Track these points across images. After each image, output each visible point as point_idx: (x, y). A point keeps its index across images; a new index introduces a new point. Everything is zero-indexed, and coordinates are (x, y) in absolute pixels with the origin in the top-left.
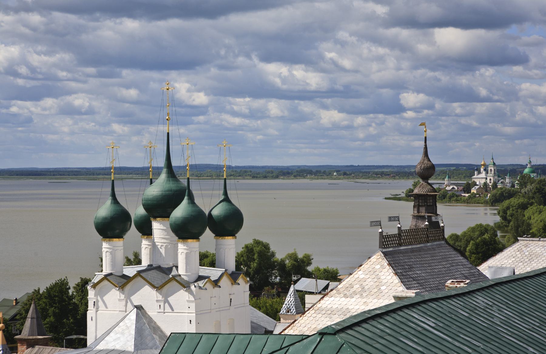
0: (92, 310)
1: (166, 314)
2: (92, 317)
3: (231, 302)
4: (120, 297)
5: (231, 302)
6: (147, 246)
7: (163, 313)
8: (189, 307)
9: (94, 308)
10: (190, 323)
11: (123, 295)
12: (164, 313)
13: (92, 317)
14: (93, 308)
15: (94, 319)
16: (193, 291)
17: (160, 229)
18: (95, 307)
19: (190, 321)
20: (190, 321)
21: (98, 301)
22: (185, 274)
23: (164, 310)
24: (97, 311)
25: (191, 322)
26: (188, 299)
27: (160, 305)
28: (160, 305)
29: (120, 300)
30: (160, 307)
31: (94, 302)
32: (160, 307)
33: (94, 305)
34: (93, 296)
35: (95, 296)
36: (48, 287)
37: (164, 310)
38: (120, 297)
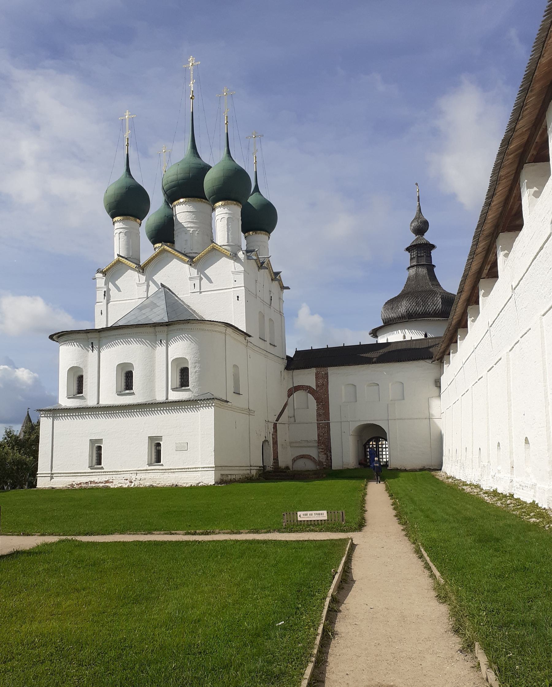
1: (203, 293)
2: (101, 310)
3: (271, 300)
4: (139, 281)
5: (271, 300)
6: (223, 216)
7: (199, 293)
8: (235, 281)
9: (104, 299)
10: (238, 300)
11: (143, 276)
12: (201, 292)
13: (101, 310)
14: (102, 300)
15: (104, 312)
16: (241, 259)
17: (187, 212)
18: (105, 297)
19: (238, 297)
20: (238, 297)
21: (109, 290)
22: (227, 244)
23: (51, 471)
24: (107, 304)
25: (239, 299)
26: (234, 270)
27: (194, 284)
28: (194, 284)
29: (138, 285)
30: (195, 286)
31: (105, 291)
32: (195, 286)
33: (105, 295)
34: (103, 285)
35: (105, 285)
36: (402, 528)
37: (51, 471)
38: (139, 281)
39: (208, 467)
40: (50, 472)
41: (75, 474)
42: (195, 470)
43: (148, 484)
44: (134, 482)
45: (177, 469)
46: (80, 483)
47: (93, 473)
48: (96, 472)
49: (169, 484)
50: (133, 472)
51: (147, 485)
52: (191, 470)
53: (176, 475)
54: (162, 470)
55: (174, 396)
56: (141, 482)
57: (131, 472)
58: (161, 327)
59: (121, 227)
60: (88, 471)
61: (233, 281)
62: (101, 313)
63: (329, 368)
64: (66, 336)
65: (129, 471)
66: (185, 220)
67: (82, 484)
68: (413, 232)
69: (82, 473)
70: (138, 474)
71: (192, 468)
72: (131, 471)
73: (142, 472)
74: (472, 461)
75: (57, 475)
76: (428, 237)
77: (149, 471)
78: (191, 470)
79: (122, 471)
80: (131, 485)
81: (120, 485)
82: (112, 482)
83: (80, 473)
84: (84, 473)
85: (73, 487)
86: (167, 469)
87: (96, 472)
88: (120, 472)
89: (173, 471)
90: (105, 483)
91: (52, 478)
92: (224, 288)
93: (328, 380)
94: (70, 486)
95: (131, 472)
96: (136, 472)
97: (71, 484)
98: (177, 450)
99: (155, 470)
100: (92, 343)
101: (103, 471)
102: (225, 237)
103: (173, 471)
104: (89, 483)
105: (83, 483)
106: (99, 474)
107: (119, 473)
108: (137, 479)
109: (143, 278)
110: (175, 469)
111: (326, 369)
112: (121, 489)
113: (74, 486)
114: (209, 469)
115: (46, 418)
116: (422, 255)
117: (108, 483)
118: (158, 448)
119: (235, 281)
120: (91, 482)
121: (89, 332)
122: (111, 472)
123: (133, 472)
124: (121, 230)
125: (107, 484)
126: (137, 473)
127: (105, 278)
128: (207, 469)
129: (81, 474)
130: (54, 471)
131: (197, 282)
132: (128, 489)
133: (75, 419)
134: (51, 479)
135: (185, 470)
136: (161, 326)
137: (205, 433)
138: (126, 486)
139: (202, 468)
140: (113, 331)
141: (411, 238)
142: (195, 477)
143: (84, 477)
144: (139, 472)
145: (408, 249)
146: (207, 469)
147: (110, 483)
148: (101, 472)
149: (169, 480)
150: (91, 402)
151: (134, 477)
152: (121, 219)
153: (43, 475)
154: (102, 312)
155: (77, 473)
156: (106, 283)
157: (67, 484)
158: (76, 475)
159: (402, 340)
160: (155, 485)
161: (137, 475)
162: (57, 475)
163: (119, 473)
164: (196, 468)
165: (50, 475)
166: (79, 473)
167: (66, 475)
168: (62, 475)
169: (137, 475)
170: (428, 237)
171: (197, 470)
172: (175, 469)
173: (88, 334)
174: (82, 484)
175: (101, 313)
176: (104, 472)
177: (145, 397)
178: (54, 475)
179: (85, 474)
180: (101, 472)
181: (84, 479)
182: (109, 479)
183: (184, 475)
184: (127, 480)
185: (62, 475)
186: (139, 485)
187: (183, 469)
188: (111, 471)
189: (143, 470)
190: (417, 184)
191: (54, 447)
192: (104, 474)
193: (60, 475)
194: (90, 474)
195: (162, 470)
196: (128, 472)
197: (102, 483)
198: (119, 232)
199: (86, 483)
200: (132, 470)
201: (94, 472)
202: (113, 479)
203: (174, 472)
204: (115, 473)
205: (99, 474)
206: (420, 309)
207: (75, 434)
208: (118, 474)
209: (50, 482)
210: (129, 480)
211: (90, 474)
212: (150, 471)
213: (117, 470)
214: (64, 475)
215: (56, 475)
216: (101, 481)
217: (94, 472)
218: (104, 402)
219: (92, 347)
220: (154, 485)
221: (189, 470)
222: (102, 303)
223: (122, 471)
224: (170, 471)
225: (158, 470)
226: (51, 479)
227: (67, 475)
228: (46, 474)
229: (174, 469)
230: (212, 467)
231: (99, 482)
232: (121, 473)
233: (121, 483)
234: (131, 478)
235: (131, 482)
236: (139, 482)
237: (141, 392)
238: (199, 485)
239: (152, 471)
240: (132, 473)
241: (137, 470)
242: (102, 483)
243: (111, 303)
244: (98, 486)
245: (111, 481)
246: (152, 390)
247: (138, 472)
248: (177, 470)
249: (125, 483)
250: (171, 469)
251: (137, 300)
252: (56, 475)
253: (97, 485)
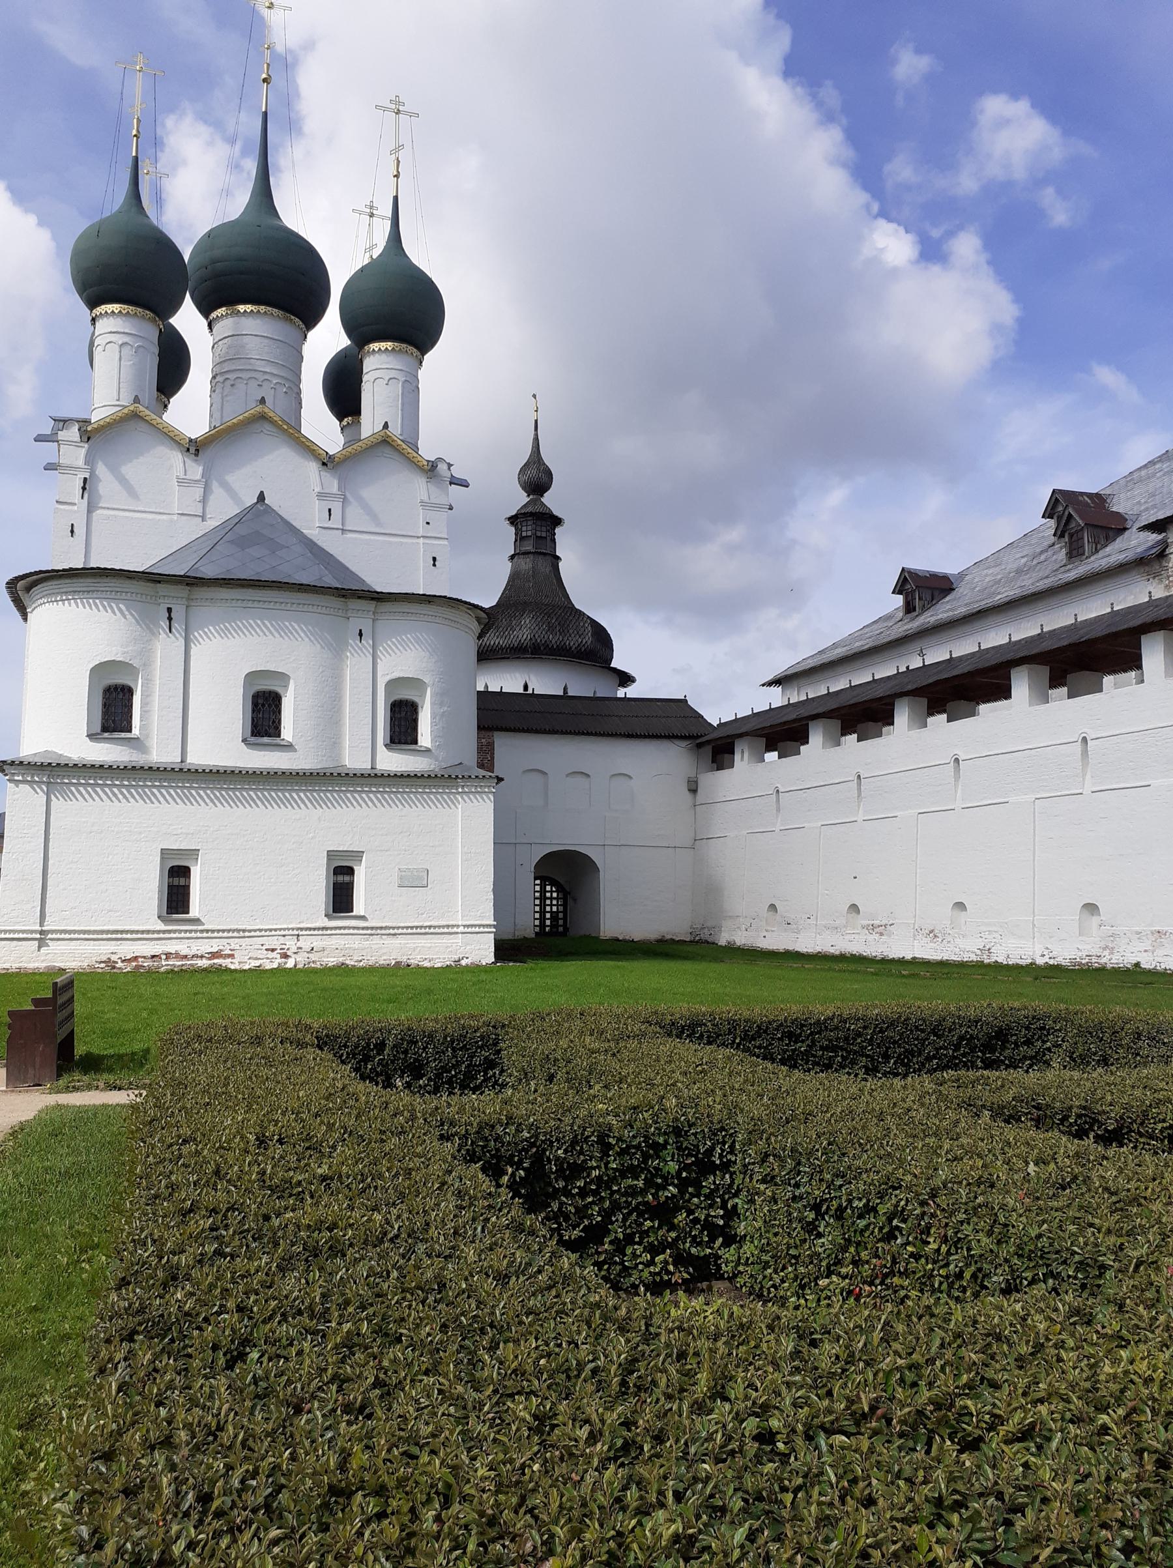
1: (350, 535)
2: (72, 525)
6: (393, 374)
8: (428, 523)
9: (82, 498)
10: (434, 565)
13: (72, 525)
15: (80, 530)
18: (86, 495)
19: (434, 559)
20: (434, 559)
23: (41, 925)
26: (426, 499)
27: (330, 510)
28: (330, 510)
29: (181, 482)
30: (330, 515)
31: (85, 479)
32: (330, 515)
33: (84, 489)
34: (80, 462)
39: (480, 926)
40: (38, 928)
41: (118, 935)
42: (446, 930)
43: (332, 961)
44: (293, 956)
45: (403, 928)
46: (136, 958)
47: (169, 932)
48: (180, 931)
49: (388, 962)
50: (286, 932)
51: (330, 964)
52: (437, 930)
53: (400, 940)
54: (363, 928)
55: (392, 761)
56: (313, 957)
57: (283, 933)
58: (359, 600)
59: (127, 331)
60: (158, 928)
61: (421, 523)
62: (72, 532)
63: (496, 734)
64: (89, 580)
65: (276, 930)
67: (140, 960)
68: (524, 488)
69: (137, 932)
70: (300, 938)
71: (439, 927)
72: (280, 930)
73: (312, 932)
74: (1034, 925)
75: (58, 936)
76: (551, 500)
77: (329, 932)
78: (437, 930)
79: (255, 931)
80: (286, 963)
81: (257, 963)
82: (232, 956)
83: (132, 932)
84: (143, 932)
85: (114, 967)
86: (377, 928)
87: (180, 931)
88: (250, 931)
89: (391, 931)
90: (209, 959)
91: (42, 943)
92: (399, 533)
93: (493, 758)
94: (103, 965)
95: (283, 933)
96: (296, 932)
97: (104, 959)
98: (402, 884)
99: (344, 928)
100: (169, 610)
101: (200, 928)
103: (391, 931)
104: (164, 957)
105: (144, 957)
106: (188, 935)
107: (247, 934)
108: (301, 948)
109: (196, 471)
110: (398, 928)
111: (490, 734)
112: (258, 972)
113: (117, 965)
114: (482, 929)
115: (27, 787)
116: (544, 535)
117: (217, 958)
118: (176, 881)
119: (428, 523)
120: (168, 955)
121: (159, 582)
122: (223, 931)
123: (286, 932)
124: (126, 339)
125: (216, 961)
126: (298, 935)
127: (86, 446)
128: (477, 930)
129: (134, 936)
130: (48, 925)
131: (337, 508)
132: (280, 971)
133: (475, 801)
134: (39, 948)
135: (423, 931)
136: (359, 598)
137: (473, 850)
138: (275, 965)
139: (464, 926)
140: (234, 590)
141: (521, 499)
142: (447, 947)
143: (144, 942)
144: (304, 932)
145: (513, 520)
146: (477, 930)
147: (224, 959)
148: (196, 931)
149: (384, 951)
150: (162, 753)
151: (291, 944)
153: (16, 936)
154: (75, 530)
155: (122, 932)
156: (90, 460)
157: (94, 959)
158: (119, 936)
159: (521, 691)
160: (352, 963)
161: (298, 940)
162: (58, 936)
163: (247, 934)
164: (448, 926)
165: (38, 936)
166: (127, 932)
167: (86, 936)
168: (72, 936)
169: (298, 940)
170: (551, 500)
171: (450, 930)
172: (398, 928)
173: (158, 585)
174: (140, 960)
175: (72, 532)
176: (202, 931)
177: (320, 758)
178: (50, 936)
179: (145, 936)
180: (196, 931)
181: (146, 949)
182: (221, 948)
183: (422, 941)
184: (273, 950)
185: (72, 936)
186: (309, 963)
187: (417, 927)
188: (225, 928)
189: (314, 929)
190: (534, 396)
191: (51, 862)
192: (205, 935)
193: (67, 936)
194: (161, 935)
195: (363, 928)
196: (273, 933)
197: (202, 957)
198: (120, 343)
199: (153, 957)
200: (285, 926)
201: (175, 931)
202: (232, 948)
203: (395, 935)
204: (235, 934)
205: (188, 935)
206: (554, 639)
207: (117, 833)
208: (244, 937)
209: (36, 953)
210: (279, 951)
211: (161, 935)
212: (333, 932)
213: (243, 927)
214: (82, 936)
215: (54, 936)
216: (199, 953)
217: (175, 931)
218: (197, 758)
219: (170, 619)
220: (348, 962)
221: (432, 930)
222: (75, 508)
223: (255, 931)
224: (383, 932)
225: (354, 928)
226: (39, 948)
227: (91, 936)
228: (23, 932)
229: (393, 928)
230: (32, 932)
231: (193, 956)
232: (253, 934)
233: (257, 959)
234: (284, 946)
235: (285, 956)
236: (307, 955)
237: (311, 745)
238: (463, 962)
239: (338, 932)
240: (284, 936)
241: (298, 929)
242: (202, 957)
243: (99, 512)
244: (192, 965)
245: (228, 952)
246: (335, 743)
247: (301, 933)
248: (400, 931)
249: (268, 958)
250: (386, 928)
251: (175, 517)
252: (54, 936)
253: (189, 963)
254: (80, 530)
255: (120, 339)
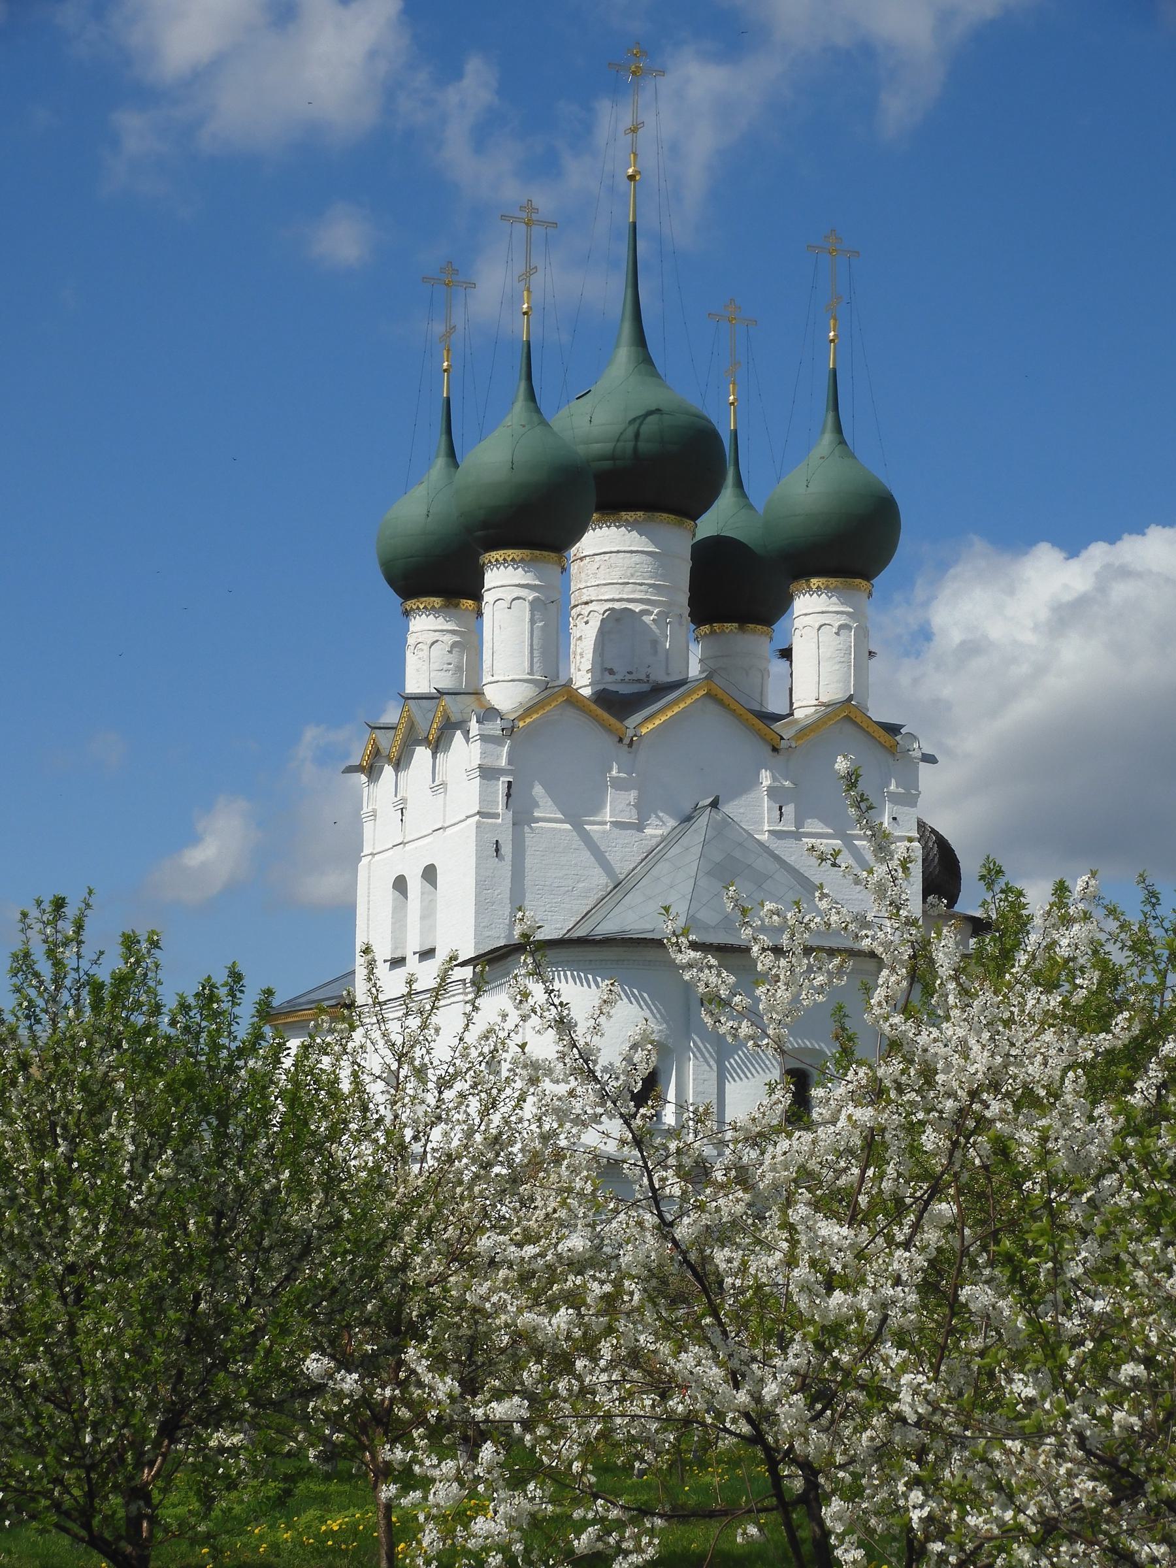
0: (496, 816)
6: (843, 620)
8: (894, 819)
14: (500, 809)
15: (507, 850)
33: (508, 795)
34: (503, 762)
62: (497, 850)
66: (651, 577)
102: (849, 682)
152: (517, 559)
254: (507, 850)
255: (532, 596)
